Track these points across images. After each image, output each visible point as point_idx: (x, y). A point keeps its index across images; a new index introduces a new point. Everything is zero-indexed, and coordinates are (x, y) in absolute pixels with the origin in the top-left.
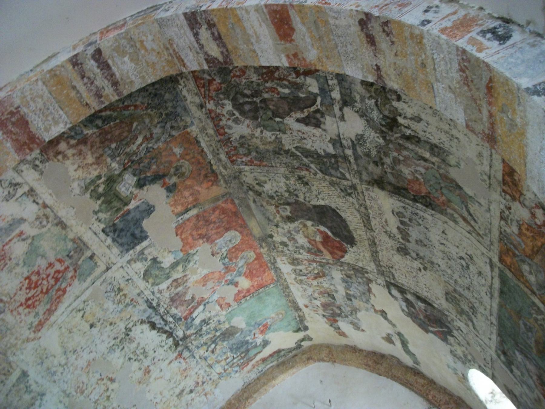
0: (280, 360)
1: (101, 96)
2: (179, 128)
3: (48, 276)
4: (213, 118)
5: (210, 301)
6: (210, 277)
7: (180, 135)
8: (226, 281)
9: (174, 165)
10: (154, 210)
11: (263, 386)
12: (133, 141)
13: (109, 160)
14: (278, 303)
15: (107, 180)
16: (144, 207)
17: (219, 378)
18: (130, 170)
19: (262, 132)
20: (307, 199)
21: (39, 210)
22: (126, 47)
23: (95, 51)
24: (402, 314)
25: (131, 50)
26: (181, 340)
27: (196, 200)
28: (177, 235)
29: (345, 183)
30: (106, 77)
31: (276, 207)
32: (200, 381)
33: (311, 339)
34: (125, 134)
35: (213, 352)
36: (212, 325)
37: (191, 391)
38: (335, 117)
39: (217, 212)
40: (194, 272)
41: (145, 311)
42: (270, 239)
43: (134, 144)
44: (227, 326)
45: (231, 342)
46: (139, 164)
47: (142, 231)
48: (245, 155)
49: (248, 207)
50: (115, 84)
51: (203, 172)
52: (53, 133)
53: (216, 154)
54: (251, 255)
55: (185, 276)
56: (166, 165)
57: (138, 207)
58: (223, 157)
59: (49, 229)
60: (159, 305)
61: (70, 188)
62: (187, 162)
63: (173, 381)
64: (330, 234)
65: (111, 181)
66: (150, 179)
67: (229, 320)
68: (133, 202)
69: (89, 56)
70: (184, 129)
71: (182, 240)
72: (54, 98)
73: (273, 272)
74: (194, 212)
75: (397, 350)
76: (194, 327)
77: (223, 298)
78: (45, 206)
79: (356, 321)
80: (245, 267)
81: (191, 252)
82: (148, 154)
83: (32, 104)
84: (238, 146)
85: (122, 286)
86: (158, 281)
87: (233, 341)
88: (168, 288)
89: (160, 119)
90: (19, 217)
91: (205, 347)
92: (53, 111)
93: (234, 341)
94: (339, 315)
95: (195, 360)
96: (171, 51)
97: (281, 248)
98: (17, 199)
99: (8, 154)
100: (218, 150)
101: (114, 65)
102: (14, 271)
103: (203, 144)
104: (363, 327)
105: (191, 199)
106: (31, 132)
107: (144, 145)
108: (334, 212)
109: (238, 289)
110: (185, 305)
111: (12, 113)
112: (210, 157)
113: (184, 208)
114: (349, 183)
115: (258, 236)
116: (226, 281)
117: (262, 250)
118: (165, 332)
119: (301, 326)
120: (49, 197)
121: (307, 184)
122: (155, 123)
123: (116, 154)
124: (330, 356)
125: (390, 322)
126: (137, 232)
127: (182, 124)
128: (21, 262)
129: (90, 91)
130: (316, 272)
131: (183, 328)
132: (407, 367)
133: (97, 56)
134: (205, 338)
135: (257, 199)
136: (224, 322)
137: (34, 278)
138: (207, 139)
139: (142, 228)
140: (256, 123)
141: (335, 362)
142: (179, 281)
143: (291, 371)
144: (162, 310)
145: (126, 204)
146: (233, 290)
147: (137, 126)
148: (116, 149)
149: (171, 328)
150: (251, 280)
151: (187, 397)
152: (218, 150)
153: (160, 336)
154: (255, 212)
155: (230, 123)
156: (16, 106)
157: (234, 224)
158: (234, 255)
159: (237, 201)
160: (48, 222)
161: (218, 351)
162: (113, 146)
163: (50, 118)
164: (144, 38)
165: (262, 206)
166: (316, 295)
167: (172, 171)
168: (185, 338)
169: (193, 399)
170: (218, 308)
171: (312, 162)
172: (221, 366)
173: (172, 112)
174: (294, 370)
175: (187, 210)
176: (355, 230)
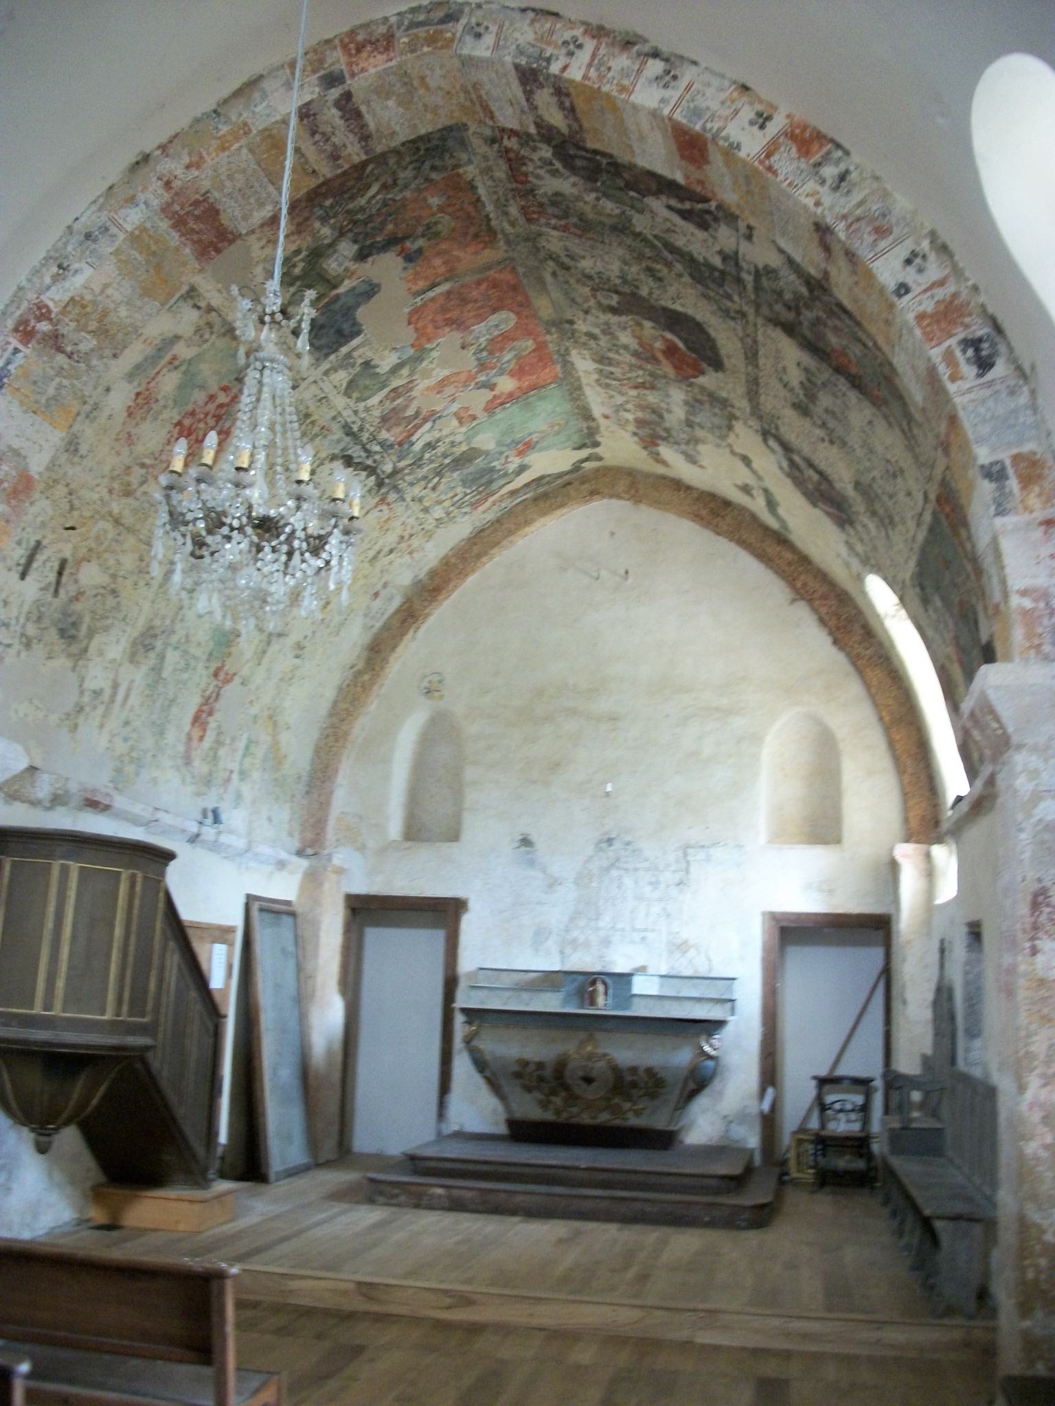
0: (541, 490)
1: (339, 158)
2: (444, 168)
3: (207, 415)
4: (510, 160)
5: (445, 414)
6: (452, 380)
7: (443, 179)
8: (477, 383)
9: (426, 222)
10: (379, 291)
11: (508, 536)
12: (362, 193)
13: (317, 224)
14: (557, 409)
15: (308, 256)
16: (364, 288)
17: (437, 526)
18: (350, 235)
19: (598, 199)
20: (654, 296)
21: (201, 317)
22: (394, 86)
23: (341, 95)
24: (778, 472)
25: (403, 90)
26: (388, 477)
27: (451, 270)
28: (409, 323)
29: (729, 304)
30: (351, 131)
31: (593, 289)
32: (406, 535)
33: (600, 459)
34: (350, 184)
35: (434, 489)
36: (441, 449)
37: (391, 551)
38: (737, 230)
39: (484, 286)
40: (427, 374)
41: (339, 441)
42: (567, 326)
43: (362, 196)
44: (464, 448)
45: (466, 471)
46: (366, 224)
47: (355, 324)
48: (556, 217)
49: (541, 281)
50: (365, 138)
51: (473, 230)
52: (255, 221)
53: (502, 207)
54: (530, 344)
55: (411, 381)
56: (413, 222)
57: (353, 289)
58: (514, 211)
59: (213, 344)
60: (361, 429)
61: (251, 276)
62: (447, 217)
63: (366, 541)
64: (681, 345)
65: (317, 254)
66: (380, 245)
67: (468, 439)
68: (347, 282)
69: (330, 104)
70: (453, 170)
71: (417, 330)
72: (263, 170)
73: (558, 367)
74: (445, 287)
75: (758, 505)
76: (411, 455)
77: (467, 409)
78: (210, 309)
79: (694, 453)
80: (514, 361)
81: (429, 346)
82: (384, 210)
83: (228, 184)
84: (547, 202)
85: (312, 409)
86: (368, 393)
87: (470, 469)
88: (381, 402)
89: (415, 158)
90: (171, 335)
91: (423, 483)
92: (259, 189)
93: (471, 469)
94: (664, 439)
95: (404, 504)
96: (474, 96)
97: (584, 339)
98: (171, 307)
99: (184, 264)
100: (507, 200)
101: (368, 112)
102: (161, 417)
103: (482, 191)
104: (704, 463)
105: (443, 269)
106: (222, 225)
107: (379, 197)
108: (699, 327)
109: (493, 393)
110: (404, 425)
111: (196, 203)
112: (490, 208)
113: (428, 283)
114: (736, 307)
115: (546, 318)
116: (477, 383)
117: (548, 337)
118: (366, 468)
119: (590, 439)
120: (217, 295)
121: (660, 279)
122: (404, 163)
123: (331, 214)
124: (633, 492)
125: (754, 472)
126: (346, 327)
127: (450, 162)
128: (170, 403)
129: (322, 151)
130: (640, 380)
131: (394, 458)
132: (766, 529)
133: (344, 102)
134: (426, 469)
135: (560, 272)
136: (460, 443)
137: (187, 422)
138: (490, 183)
139: (355, 319)
140: (589, 185)
141: (640, 502)
142: (401, 390)
143: (558, 512)
144: (365, 436)
145: (335, 287)
146: (487, 395)
147: (373, 169)
148: (332, 207)
149: (375, 461)
150: (519, 379)
151: (383, 561)
152: (507, 200)
153: (356, 475)
154: (550, 288)
155: (541, 172)
156: (203, 191)
157: (510, 301)
158: (498, 346)
159: (521, 270)
160: (212, 333)
161: (442, 487)
162: (328, 203)
163: (252, 200)
164: (428, 72)
165: (567, 282)
166: (629, 406)
167: (420, 230)
168: (395, 472)
169: (391, 563)
170: (455, 423)
171: (678, 261)
172: (443, 508)
173: (437, 146)
174: (565, 510)
175: (433, 286)
176: (729, 357)
